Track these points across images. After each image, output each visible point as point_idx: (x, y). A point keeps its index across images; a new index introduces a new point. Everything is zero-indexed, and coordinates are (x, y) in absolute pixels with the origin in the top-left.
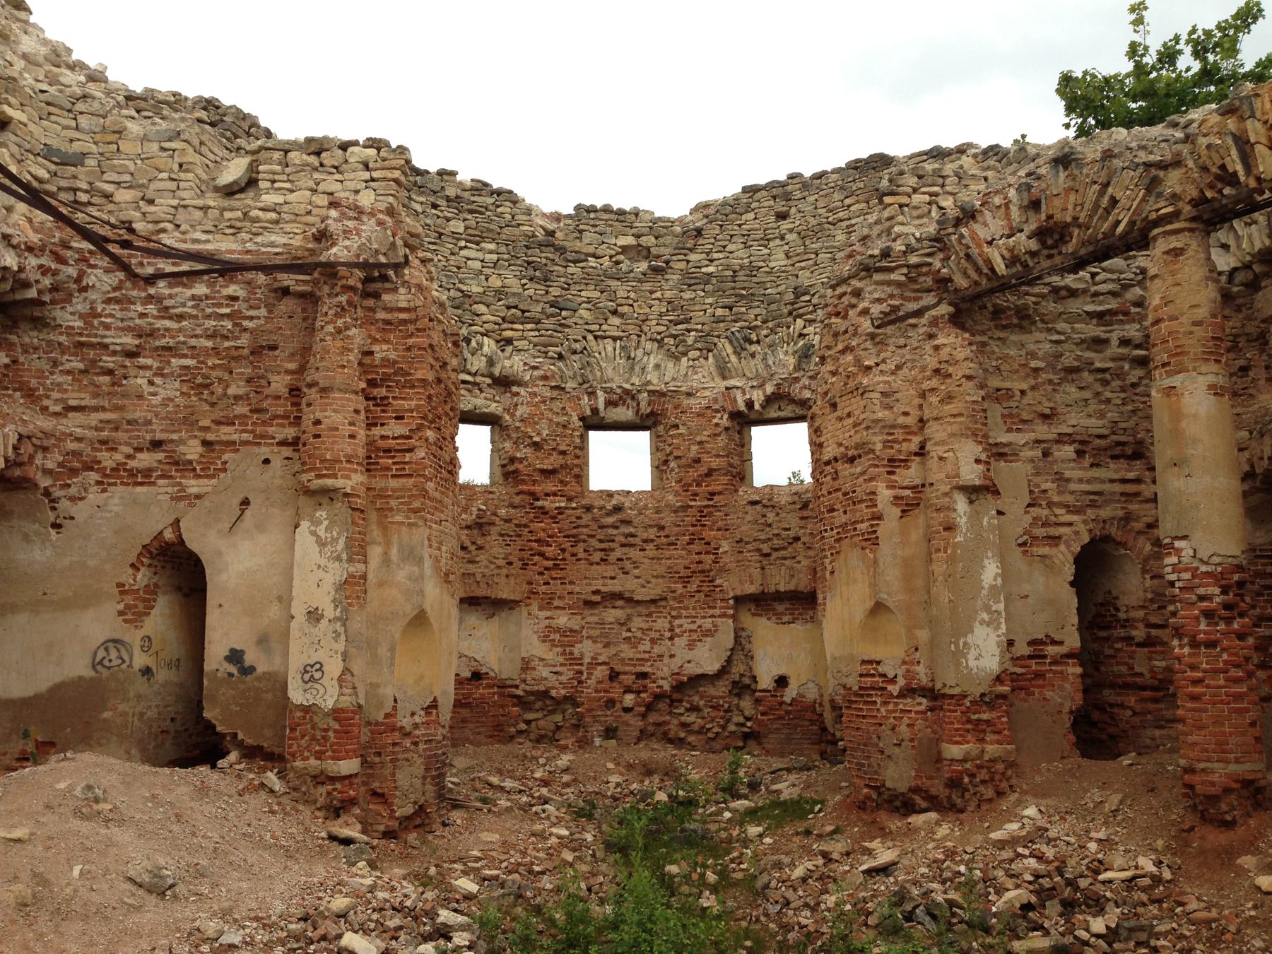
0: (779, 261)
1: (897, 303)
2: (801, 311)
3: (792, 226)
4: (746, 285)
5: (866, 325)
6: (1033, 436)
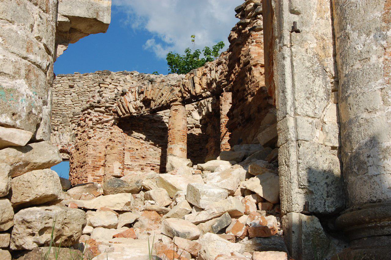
0: (69, 102)
1: (101, 118)
2: (74, 121)
3: (74, 91)
4: (55, 109)
5: (91, 123)
6: (139, 163)
